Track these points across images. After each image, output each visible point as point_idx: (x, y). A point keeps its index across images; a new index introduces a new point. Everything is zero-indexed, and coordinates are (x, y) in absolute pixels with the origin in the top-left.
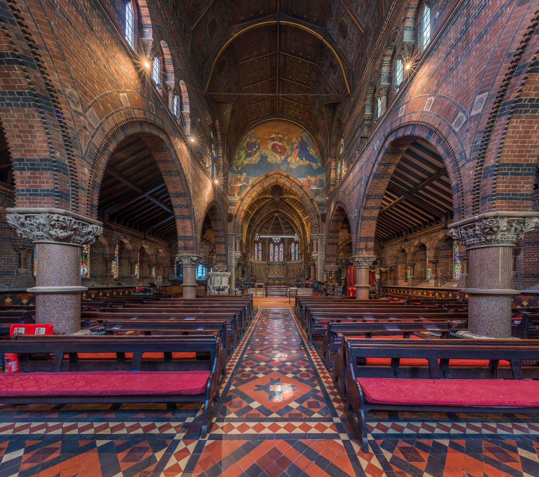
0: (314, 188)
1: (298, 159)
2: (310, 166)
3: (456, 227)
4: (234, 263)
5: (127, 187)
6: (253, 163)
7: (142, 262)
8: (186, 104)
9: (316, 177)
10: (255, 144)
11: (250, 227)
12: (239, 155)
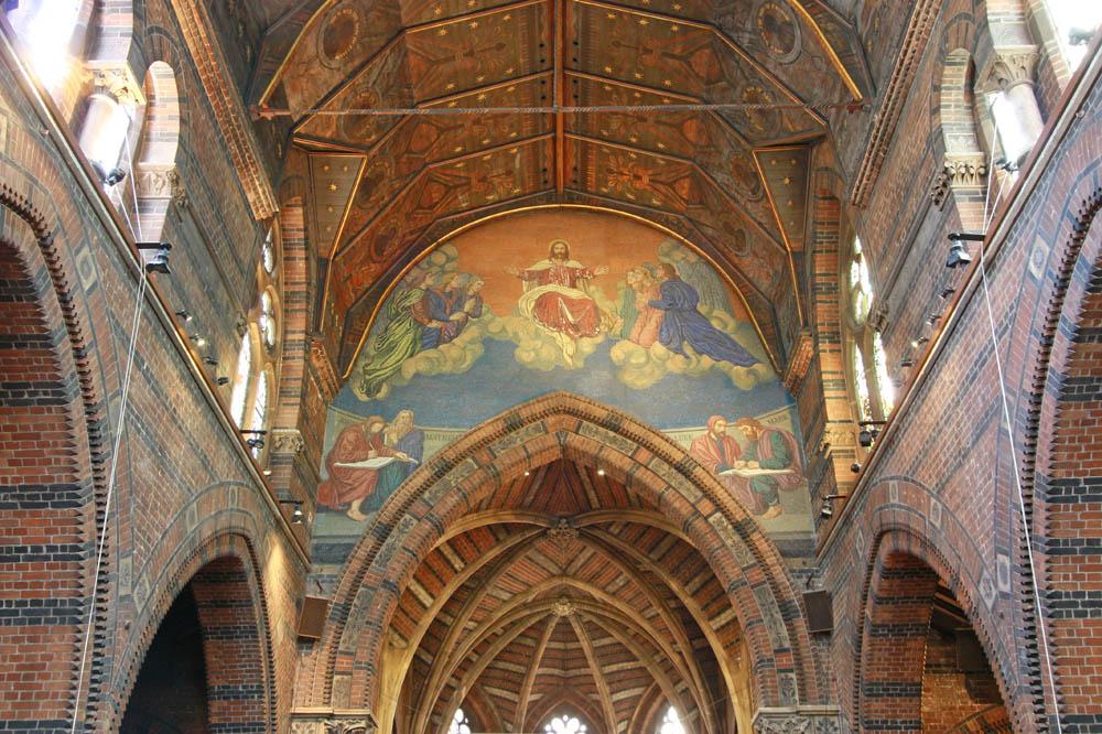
0: (753, 470)
1: (659, 349)
6: (447, 368)
8: (165, 138)
10: (458, 298)
11: (419, 674)
12: (383, 339)
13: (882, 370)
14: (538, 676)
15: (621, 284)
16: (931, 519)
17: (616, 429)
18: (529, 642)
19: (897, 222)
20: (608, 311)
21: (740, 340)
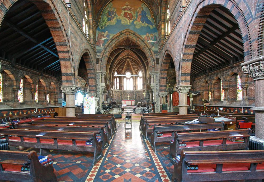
0: (151, 41)
1: (141, 22)
2: (148, 27)
3: (246, 65)
4: (101, 91)
5: (27, 39)
6: (112, 24)
7: (39, 91)
9: (152, 35)
10: (113, 12)
12: (103, 19)
13: (169, 27)
14: (125, 68)
15: (136, 11)
16: (171, 49)
18: (124, 63)
19: (174, 3)
20: (134, 15)
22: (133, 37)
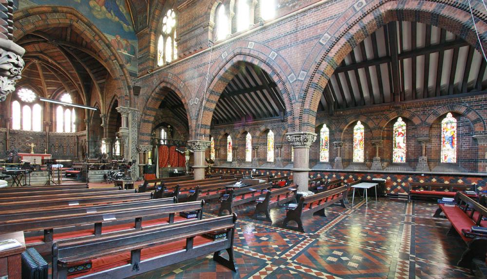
1: (104, 8)
9: (127, 42)
17: (90, 27)
21: (127, 17)
22: (84, 30)
